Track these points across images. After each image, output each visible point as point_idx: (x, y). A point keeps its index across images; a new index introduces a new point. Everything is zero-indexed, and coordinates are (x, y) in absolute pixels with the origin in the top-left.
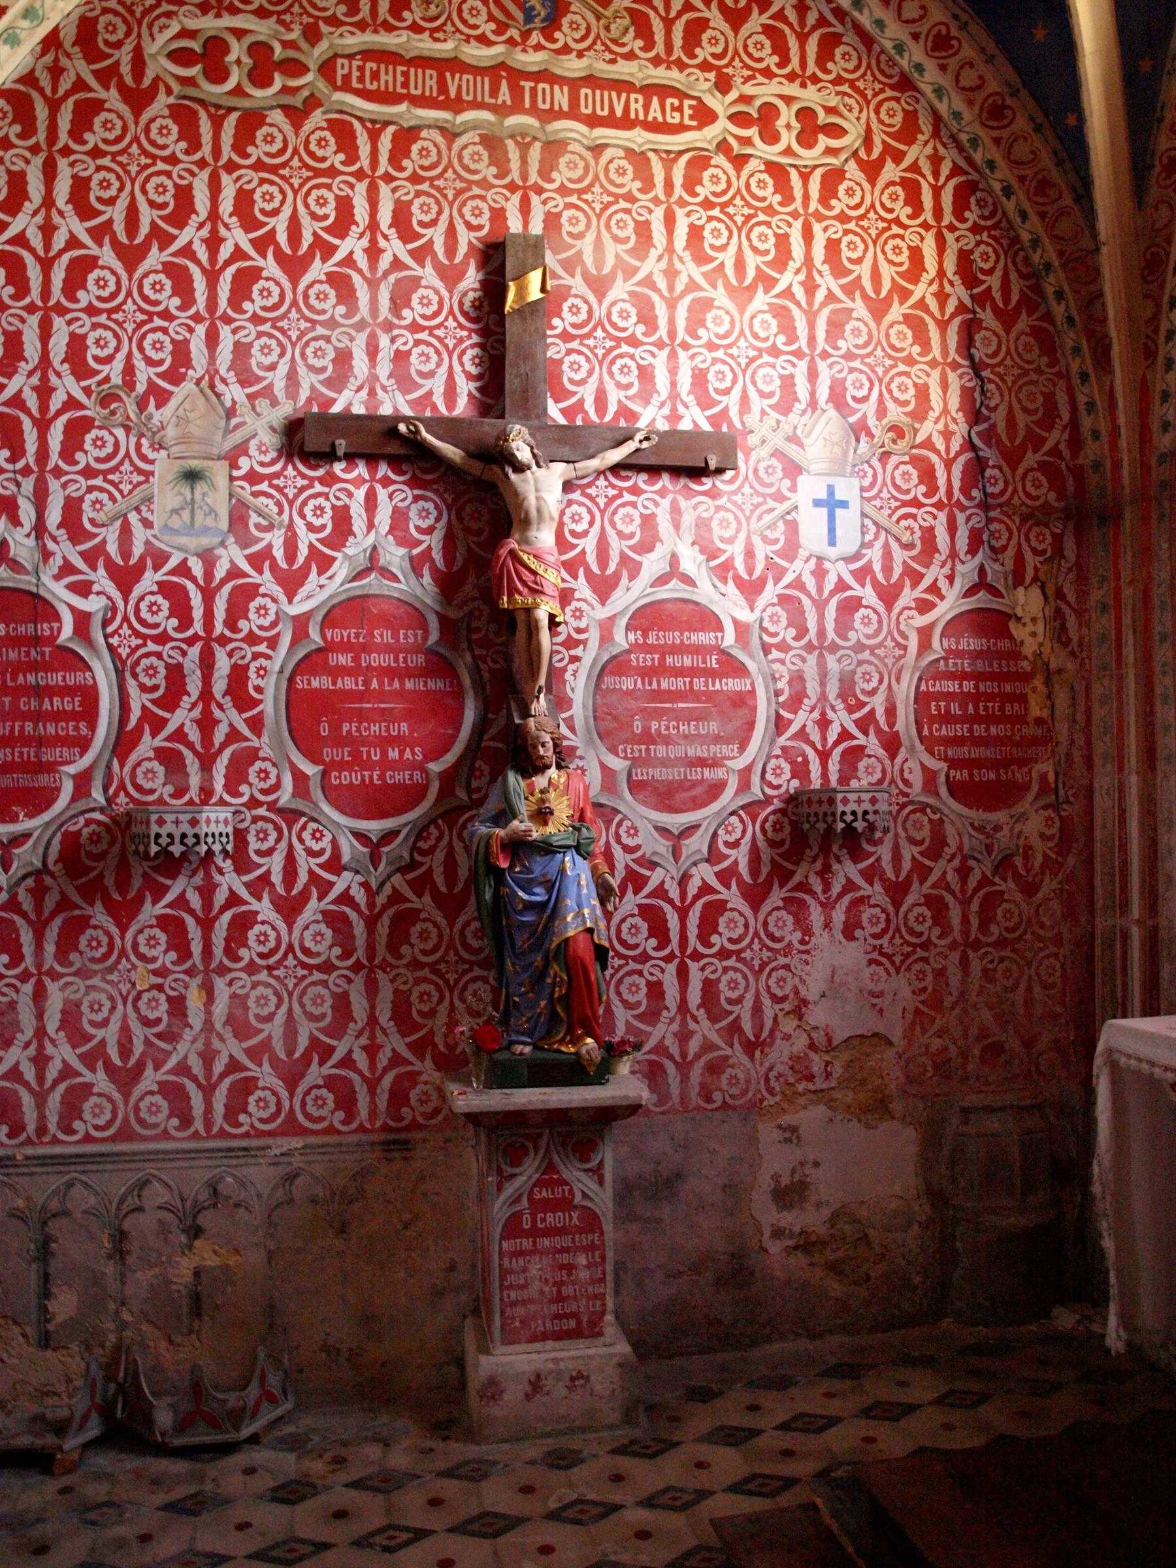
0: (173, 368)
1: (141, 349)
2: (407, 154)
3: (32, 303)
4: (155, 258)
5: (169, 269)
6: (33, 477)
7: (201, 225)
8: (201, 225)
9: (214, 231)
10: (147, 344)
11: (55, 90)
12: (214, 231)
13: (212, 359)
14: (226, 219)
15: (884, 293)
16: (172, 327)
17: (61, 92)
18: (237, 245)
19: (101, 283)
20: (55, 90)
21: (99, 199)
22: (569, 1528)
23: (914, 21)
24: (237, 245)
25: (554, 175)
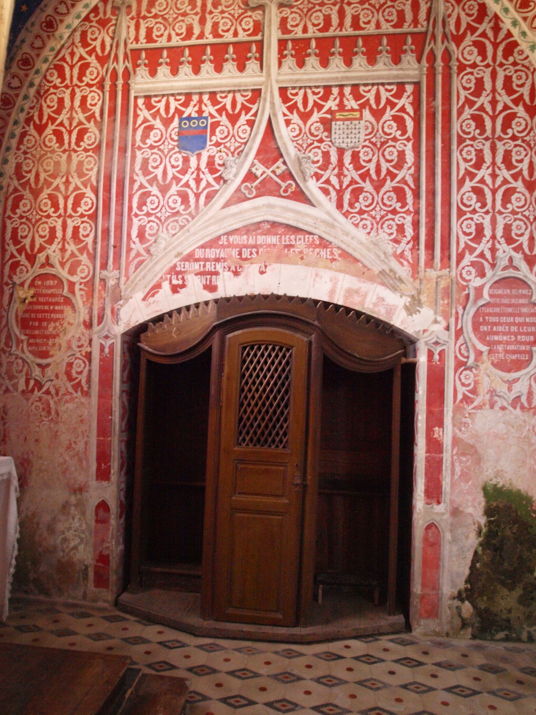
0: (323, 165)
1: (384, 156)
2: (85, 75)
3: (487, 137)
4: (389, 114)
5: (395, 118)
6: (490, 215)
7: (195, 106)
8: (195, 106)
9: (494, 97)
10: (386, 153)
11: (72, 62)
12: (494, 97)
13: (494, 158)
14: (348, 97)
15: (237, 111)
16: (397, 144)
17: (74, 62)
18: (505, 104)
19: (222, 132)
20: (72, 62)
21: (291, 94)
22: (295, 672)
23: (67, 7)
24: (505, 104)
25: (84, 78)
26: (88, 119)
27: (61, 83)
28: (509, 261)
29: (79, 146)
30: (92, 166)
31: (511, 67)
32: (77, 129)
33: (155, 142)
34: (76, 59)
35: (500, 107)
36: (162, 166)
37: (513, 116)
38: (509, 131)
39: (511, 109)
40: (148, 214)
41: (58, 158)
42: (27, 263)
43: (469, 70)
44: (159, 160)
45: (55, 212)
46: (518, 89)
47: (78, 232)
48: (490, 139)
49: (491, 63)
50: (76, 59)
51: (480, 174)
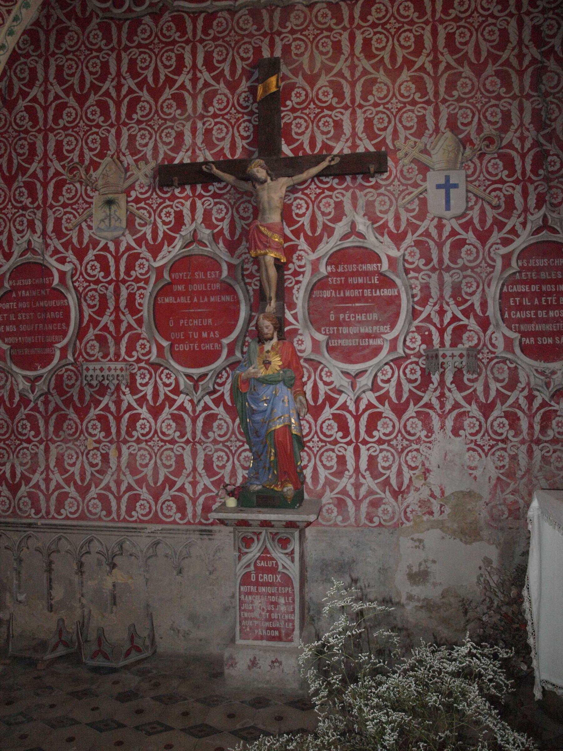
11: (48, 26)
14: (124, 75)
18: (129, 87)
19: (220, 102)
26: (67, 92)
27: (106, 45)
28: (543, 221)
29: (367, 100)
30: (146, 140)
31: (540, 15)
32: (203, 92)
33: (220, 110)
34: (52, 23)
35: (124, 91)
36: (309, 132)
37: (138, 100)
38: (211, 109)
39: (371, 74)
40: (64, 205)
41: (340, 116)
42: (149, 255)
43: (22, 60)
44: (386, 120)
45: (32, 203)
46: (68, 78)
47: (61, 224)
48: (349, 107)
49: (116, 47)
50: (52, 23)
51: (33, 167)
